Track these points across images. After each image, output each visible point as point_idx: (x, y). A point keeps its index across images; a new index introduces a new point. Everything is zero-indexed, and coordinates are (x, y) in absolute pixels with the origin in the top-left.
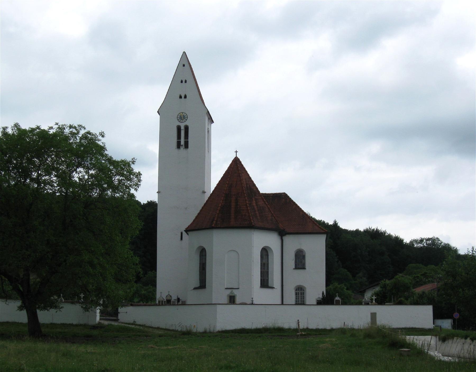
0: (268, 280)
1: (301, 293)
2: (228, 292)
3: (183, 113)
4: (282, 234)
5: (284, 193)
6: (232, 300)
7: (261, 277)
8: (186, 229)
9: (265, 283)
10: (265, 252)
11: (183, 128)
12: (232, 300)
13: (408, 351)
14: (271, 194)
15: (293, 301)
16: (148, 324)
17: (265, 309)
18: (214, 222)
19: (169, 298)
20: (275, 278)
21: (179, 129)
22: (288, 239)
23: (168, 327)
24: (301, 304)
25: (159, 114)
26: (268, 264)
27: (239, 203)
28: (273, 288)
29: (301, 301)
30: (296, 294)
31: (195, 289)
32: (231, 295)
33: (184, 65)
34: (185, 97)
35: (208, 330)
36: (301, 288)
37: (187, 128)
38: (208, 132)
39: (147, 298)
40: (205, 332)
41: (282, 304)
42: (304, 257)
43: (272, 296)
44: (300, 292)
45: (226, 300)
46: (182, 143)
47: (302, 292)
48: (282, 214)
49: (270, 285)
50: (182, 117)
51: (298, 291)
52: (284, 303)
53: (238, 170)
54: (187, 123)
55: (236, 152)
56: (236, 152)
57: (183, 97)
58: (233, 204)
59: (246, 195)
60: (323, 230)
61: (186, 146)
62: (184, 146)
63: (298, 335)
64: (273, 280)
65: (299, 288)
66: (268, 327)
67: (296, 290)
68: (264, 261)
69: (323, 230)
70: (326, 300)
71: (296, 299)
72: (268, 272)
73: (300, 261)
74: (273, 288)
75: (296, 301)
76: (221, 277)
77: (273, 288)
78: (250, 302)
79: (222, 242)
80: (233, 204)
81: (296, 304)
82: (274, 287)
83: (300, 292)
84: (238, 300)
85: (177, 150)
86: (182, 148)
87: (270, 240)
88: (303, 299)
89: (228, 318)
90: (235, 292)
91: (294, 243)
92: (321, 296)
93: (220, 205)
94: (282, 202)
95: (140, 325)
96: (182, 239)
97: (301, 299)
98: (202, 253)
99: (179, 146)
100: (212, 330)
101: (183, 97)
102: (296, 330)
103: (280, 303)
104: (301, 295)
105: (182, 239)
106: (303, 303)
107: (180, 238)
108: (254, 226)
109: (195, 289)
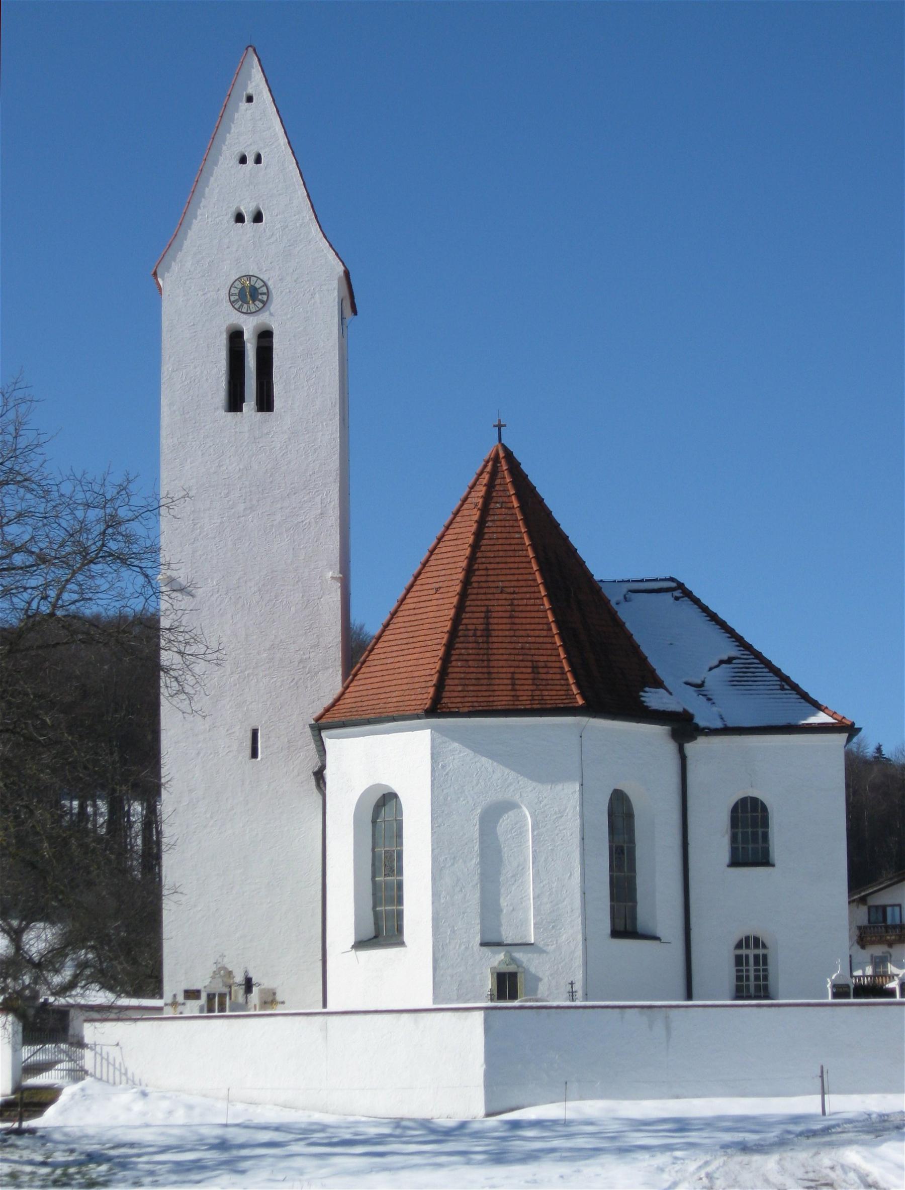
1: (756, 957)
3: (249, 277)
10: (383, 809)
21: (236, 338)
30: (739, 960)
34: (258, 218)
36: (757, 940)
37: (265, 337)
42: (764, 821)
44: (751, 952)
47: (760, 952)
51: (743, 952)
55: (500, 426)
56: (500, 426)
61: (265, 403)
71: (739, 978)
73: (751, 835)
74: (657, 939)
88: (766, 978)
91: (727, 768)
96: (254, 754)
97: (757, 978)
99: (235, 403)
104: (757, 963)
105: (254, 754)
107: (248, 751)
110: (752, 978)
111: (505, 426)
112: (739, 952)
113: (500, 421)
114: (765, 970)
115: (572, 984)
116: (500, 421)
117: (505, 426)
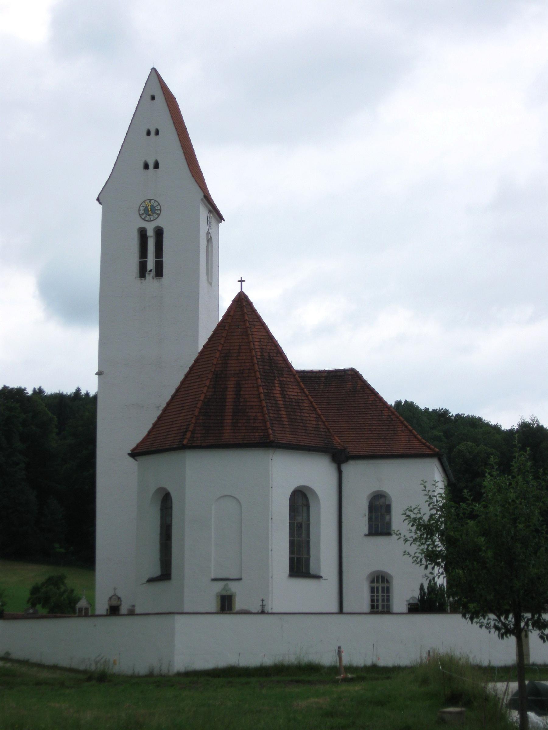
0: (308, 560)
2: (218, 587)
3: (150, 200)
4: (340, 458)
5: (353, 370)
6: (226, 604)
7: (292, 552)
8: (133, 450)
9: (300, 566)
10: (301, 500)
11: (150, 233)
12: (226, 604)
13: (460, 713)
14: (320, 372)
15: (366, 606)
16: (35, 658)
17: (304, 623)
18: (188, 435)
19: (115, 603)
20: (324, 555)
21: (143, 234)
22: (354, 471)
23: (75, 665)
24: (383, 613)
25: (100, 203)
26: (308, 525)
27: (244, 390)
28: (318, 577)
29: (383, 606)
30: (372, 590)
31: (151, 580)
32: (224, 593)
33: (153, 98)
34: (156, 166)
35: (156, 671)
36: (383, 578)
37: (159, 233)
38: (209, 240)
39: (55, 603)
40: (151, 675)
41: (341, 611)
43: (317, 594)
44: (380, 585)
45: (213, 605)
46: (151, 264)
47: (385, 585)
48: (342, 414)
49: (313, 570)
50: (150, 210)
51: (375, 585)
52: (345, 610)
53: (245, 321)
54: (160, 222)
56: (241, 281)
57: (151, 166)
58: (230, 395)
59: (258, 373)
60: (429, 448)
61: (159, 272)
62: (153, 273)
63: (338, 680)
64: (318, 560)
65: (378, 578)
66: (286, 663)
67: (372, 582)
68: (299, 519)
69: (429, 448)
70: (428, 603)
71: (372, 601)
72: (308, 542)
74: (318, 577)
75: (372, 607)
76: (201, 556)
77: (318, 577)
78: (259, 609)
79: (207, 479)
80: (230, 395)
81: (372, 613)
82: (321, 574)
83: (380, 584)
84: (238, 605)
85: (138, 281)
86: (149, 277)
87: (313, 472)
89: (200, 643)
90: (234, 587)
91: (366, 478)
92: (417, 594)
93: (202, 398)
94: (346, 386)
95: (18, 661)
97: (383, 600)
98: (166, 502)
99: (143, 271)
100: (164, 671)
101: (151, 166)
102: (334, 670)
103: (335, 609)
104: (383, 591)
106: (387, 610)
108: (273, 442)
109: (151, 580)
110: (380, 599)
111: (244, 281)
112: (373, 585)
113: (241, 278)
114: (388, 596)
115: (263, 600)
116: (241, 278)
117: (244, 281)
